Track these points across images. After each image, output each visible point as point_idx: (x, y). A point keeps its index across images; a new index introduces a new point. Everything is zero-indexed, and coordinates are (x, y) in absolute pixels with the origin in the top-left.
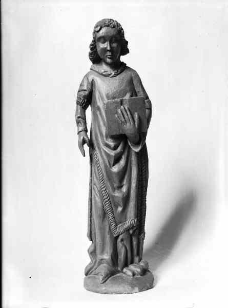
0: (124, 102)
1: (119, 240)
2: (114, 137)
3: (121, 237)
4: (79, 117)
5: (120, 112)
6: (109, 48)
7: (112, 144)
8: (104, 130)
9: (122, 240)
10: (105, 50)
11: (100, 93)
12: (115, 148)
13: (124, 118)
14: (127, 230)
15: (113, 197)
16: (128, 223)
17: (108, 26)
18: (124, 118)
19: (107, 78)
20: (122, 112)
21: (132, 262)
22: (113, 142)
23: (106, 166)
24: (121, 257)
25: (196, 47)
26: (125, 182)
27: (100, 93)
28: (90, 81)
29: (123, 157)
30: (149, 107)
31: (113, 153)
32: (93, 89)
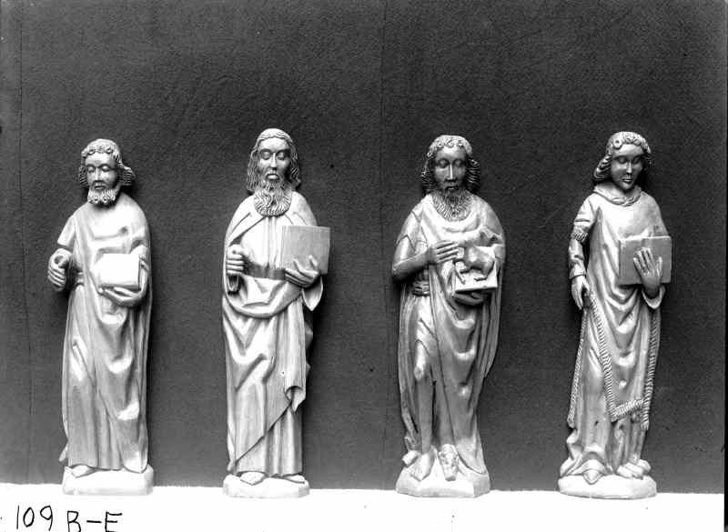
0: (646, 243)
1: (618, 426)
2: (623, 287)
3: (620, 423)
4: (143, 259)
5: (640, 255)
6: (630, 171)
7: (623, 296)
8: (612, 277)
9: (622, 427)
10: (625, 173)
11: (608, 225)
12: (627, 300)
13: (646, 263)
14: (630, 413)
15: (618, 367)
16: (631, 404)
17: (632, 143)
18: (646, 263)
19: (620, 206)
20: (643, 255)
21: (628, 461)
22: (624, 293)
23: (610, 324)
24: (618, 452)
25: (365, 507)
26: (632, 348)
27: (609, 229)
28: (595, 209)
29: (633, 312)
30: (108, 524)
31: (624, 308)
32: (599, 221)
